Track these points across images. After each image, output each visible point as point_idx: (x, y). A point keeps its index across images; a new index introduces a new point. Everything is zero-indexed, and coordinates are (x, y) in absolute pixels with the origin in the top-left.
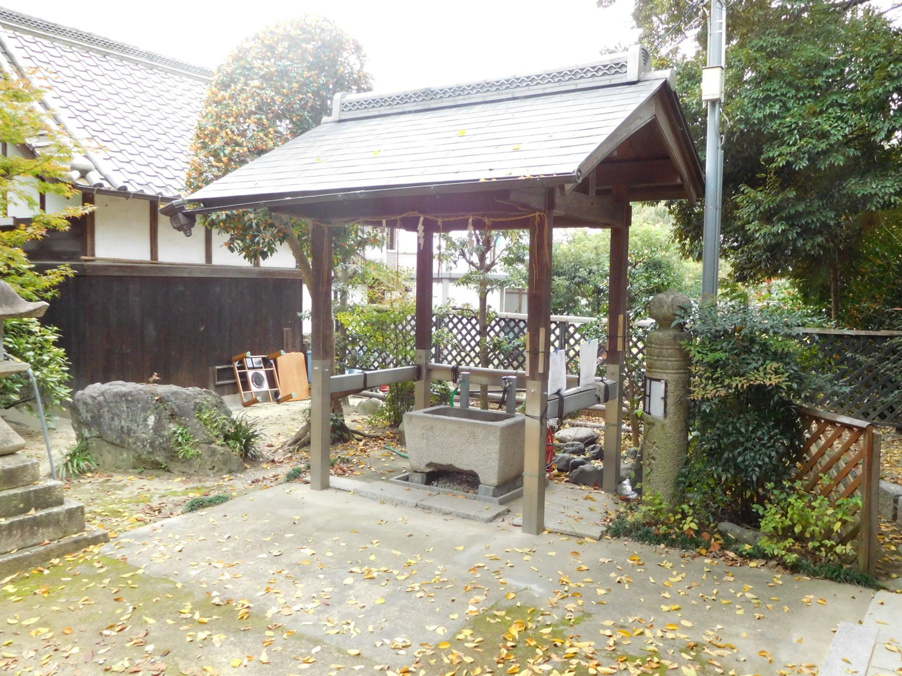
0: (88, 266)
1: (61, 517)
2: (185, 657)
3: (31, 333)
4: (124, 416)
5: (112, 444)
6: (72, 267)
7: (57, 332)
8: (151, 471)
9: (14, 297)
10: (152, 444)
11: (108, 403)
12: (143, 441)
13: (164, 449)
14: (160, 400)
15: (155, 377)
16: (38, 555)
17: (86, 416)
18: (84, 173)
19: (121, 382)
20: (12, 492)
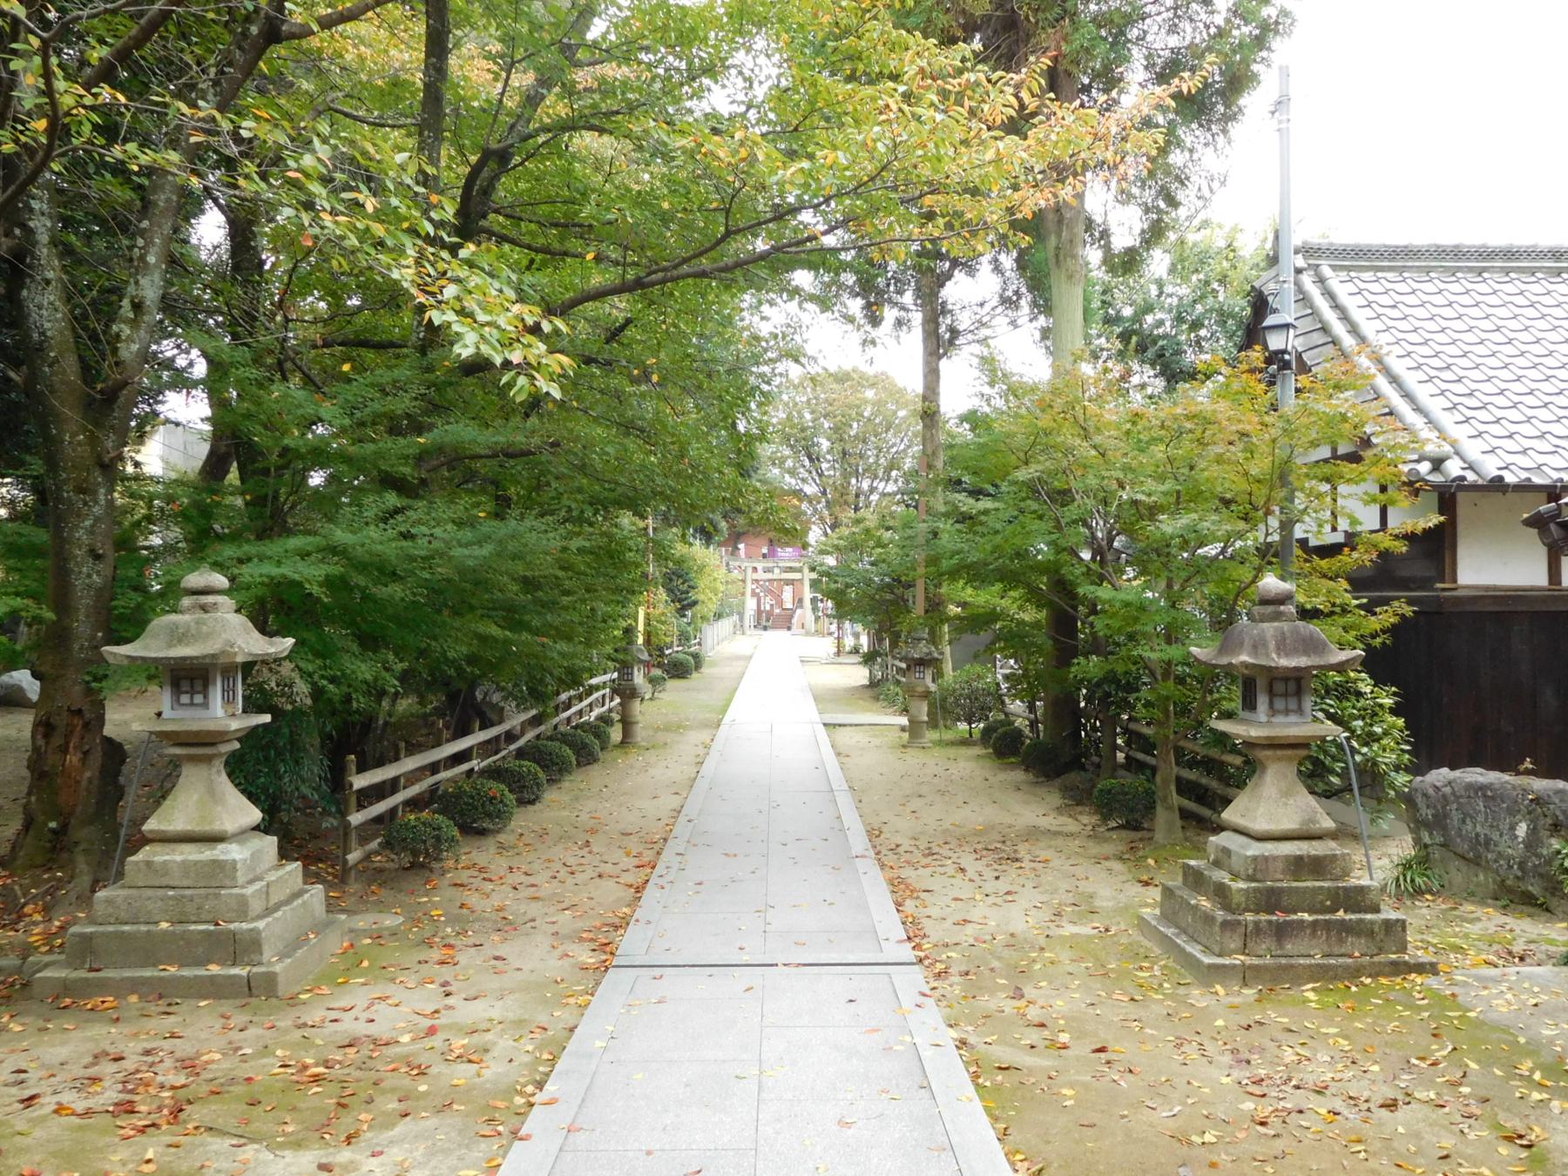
0: (1446, 598)
1: (1376, 929)
2: (1508, 1110)
3: (1359, 694)
4: (1480, 818)
5: (1464, 858)
6: (1410, 602)
7: (1395, 694)
8: (1521, 907)
9: (1325, 644)
10: (1522, 865)
11: (1457, 798)
12: (1509, 858)
13: (1541, 876)
14: (1537, 801)
15: (1528, 764)
16: (1346, 968)
17: (1427, 813)
18: (1438, 463)
19: (1479, 770)
20: (1318, 884)
